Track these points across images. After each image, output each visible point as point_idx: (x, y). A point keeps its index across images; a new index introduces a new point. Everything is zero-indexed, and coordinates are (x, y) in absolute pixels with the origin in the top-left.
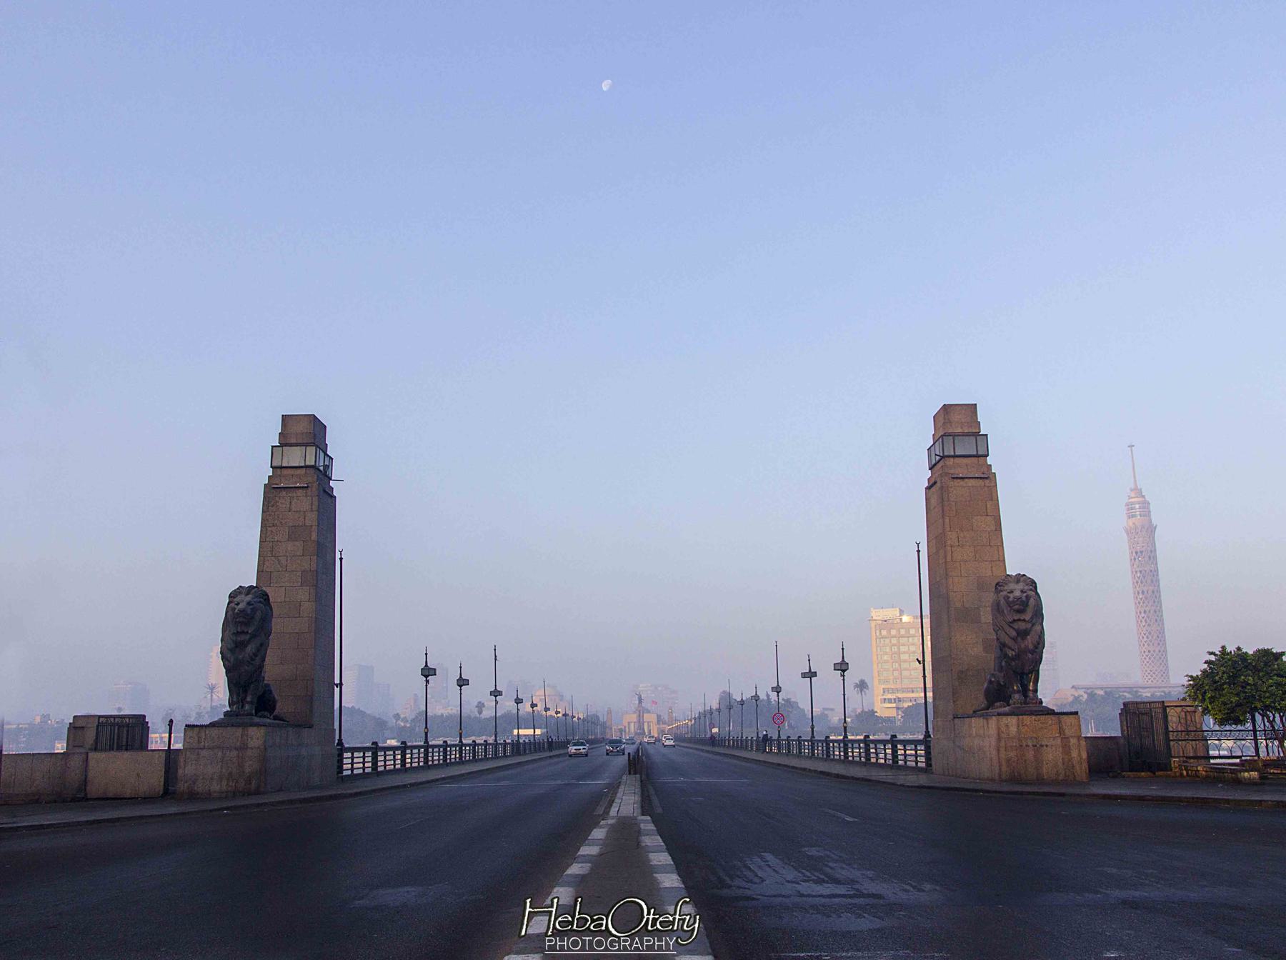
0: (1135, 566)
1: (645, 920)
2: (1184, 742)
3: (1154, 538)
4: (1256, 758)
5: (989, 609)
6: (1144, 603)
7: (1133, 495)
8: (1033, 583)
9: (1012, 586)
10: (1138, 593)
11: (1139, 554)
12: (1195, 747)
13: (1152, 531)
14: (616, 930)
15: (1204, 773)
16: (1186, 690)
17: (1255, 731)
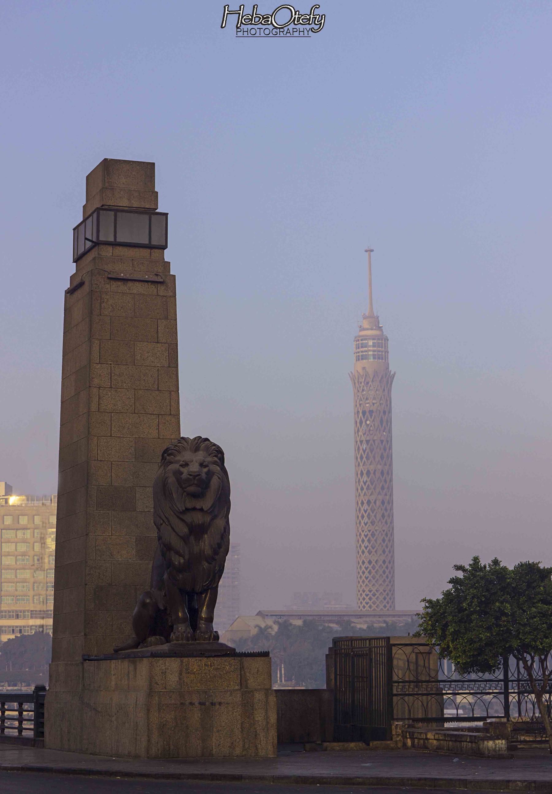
0: (360, 433)
1: (293, 18)
2: (411, 698)
3: (389, 391)
4: (505, 720)
5: (150, 490)
6: (368, 488)
7: (366, 324)
8: (219, 453)
9: (187, 456)
10: (362, 474)
11: (367, 414)
12: (425, 705)
13: (387, 382)
14: (277, 24)
15: (435, 742)
16: (421, 621)
17: (506, 680)
